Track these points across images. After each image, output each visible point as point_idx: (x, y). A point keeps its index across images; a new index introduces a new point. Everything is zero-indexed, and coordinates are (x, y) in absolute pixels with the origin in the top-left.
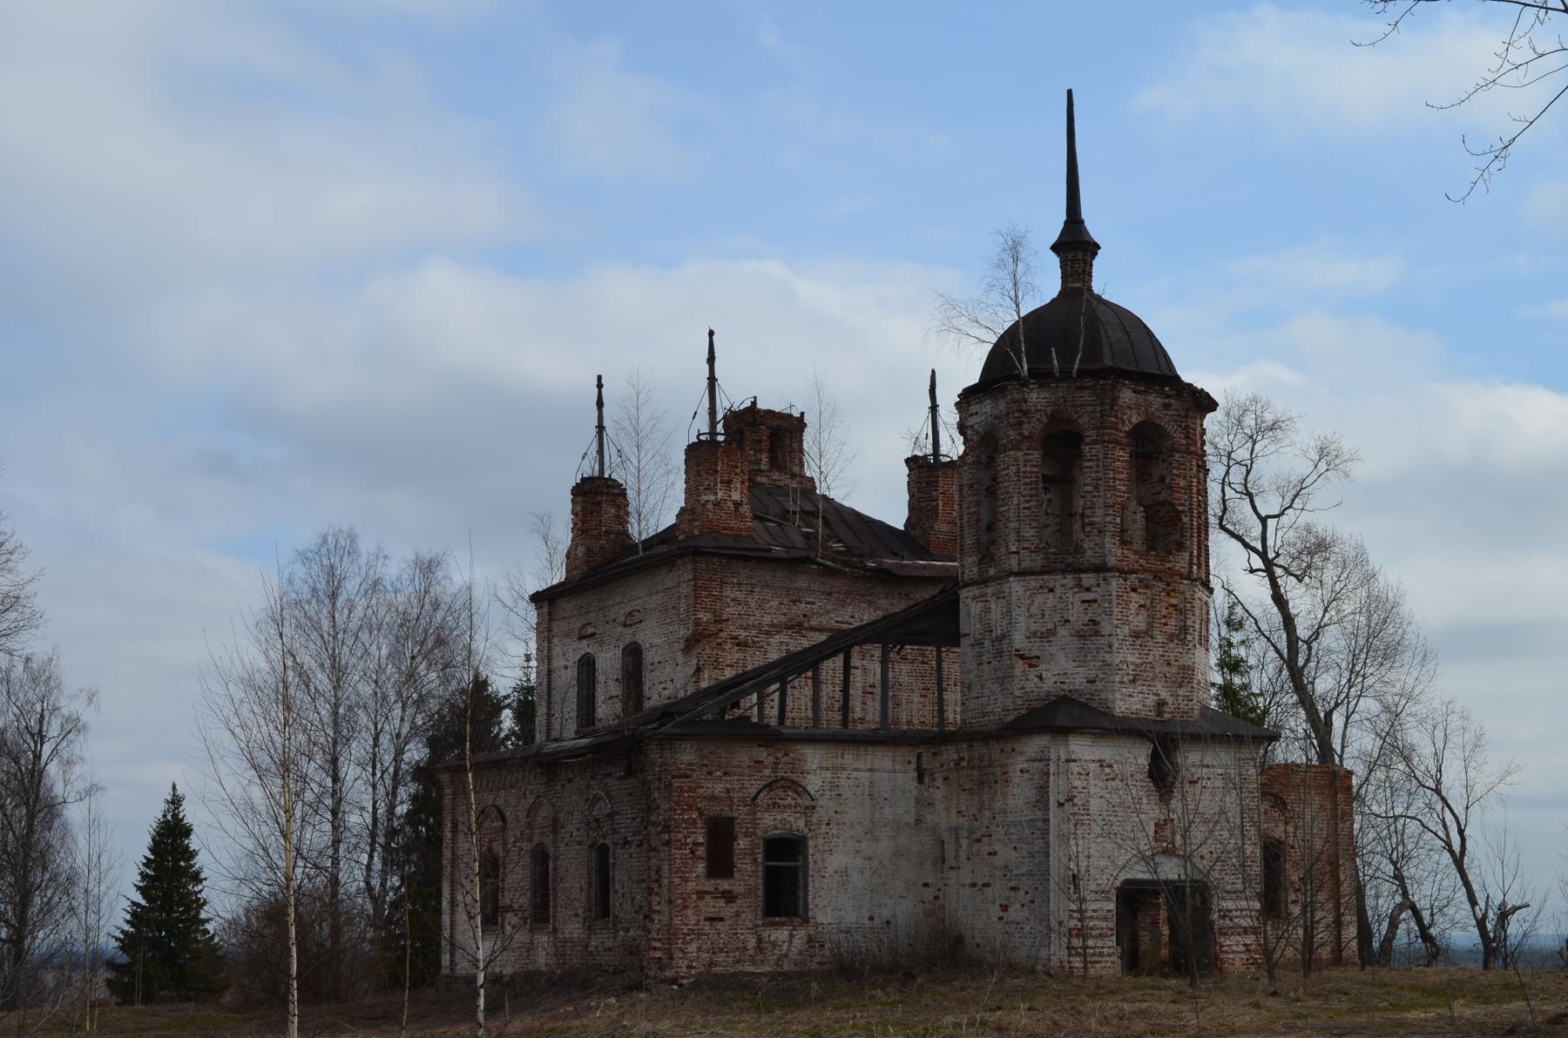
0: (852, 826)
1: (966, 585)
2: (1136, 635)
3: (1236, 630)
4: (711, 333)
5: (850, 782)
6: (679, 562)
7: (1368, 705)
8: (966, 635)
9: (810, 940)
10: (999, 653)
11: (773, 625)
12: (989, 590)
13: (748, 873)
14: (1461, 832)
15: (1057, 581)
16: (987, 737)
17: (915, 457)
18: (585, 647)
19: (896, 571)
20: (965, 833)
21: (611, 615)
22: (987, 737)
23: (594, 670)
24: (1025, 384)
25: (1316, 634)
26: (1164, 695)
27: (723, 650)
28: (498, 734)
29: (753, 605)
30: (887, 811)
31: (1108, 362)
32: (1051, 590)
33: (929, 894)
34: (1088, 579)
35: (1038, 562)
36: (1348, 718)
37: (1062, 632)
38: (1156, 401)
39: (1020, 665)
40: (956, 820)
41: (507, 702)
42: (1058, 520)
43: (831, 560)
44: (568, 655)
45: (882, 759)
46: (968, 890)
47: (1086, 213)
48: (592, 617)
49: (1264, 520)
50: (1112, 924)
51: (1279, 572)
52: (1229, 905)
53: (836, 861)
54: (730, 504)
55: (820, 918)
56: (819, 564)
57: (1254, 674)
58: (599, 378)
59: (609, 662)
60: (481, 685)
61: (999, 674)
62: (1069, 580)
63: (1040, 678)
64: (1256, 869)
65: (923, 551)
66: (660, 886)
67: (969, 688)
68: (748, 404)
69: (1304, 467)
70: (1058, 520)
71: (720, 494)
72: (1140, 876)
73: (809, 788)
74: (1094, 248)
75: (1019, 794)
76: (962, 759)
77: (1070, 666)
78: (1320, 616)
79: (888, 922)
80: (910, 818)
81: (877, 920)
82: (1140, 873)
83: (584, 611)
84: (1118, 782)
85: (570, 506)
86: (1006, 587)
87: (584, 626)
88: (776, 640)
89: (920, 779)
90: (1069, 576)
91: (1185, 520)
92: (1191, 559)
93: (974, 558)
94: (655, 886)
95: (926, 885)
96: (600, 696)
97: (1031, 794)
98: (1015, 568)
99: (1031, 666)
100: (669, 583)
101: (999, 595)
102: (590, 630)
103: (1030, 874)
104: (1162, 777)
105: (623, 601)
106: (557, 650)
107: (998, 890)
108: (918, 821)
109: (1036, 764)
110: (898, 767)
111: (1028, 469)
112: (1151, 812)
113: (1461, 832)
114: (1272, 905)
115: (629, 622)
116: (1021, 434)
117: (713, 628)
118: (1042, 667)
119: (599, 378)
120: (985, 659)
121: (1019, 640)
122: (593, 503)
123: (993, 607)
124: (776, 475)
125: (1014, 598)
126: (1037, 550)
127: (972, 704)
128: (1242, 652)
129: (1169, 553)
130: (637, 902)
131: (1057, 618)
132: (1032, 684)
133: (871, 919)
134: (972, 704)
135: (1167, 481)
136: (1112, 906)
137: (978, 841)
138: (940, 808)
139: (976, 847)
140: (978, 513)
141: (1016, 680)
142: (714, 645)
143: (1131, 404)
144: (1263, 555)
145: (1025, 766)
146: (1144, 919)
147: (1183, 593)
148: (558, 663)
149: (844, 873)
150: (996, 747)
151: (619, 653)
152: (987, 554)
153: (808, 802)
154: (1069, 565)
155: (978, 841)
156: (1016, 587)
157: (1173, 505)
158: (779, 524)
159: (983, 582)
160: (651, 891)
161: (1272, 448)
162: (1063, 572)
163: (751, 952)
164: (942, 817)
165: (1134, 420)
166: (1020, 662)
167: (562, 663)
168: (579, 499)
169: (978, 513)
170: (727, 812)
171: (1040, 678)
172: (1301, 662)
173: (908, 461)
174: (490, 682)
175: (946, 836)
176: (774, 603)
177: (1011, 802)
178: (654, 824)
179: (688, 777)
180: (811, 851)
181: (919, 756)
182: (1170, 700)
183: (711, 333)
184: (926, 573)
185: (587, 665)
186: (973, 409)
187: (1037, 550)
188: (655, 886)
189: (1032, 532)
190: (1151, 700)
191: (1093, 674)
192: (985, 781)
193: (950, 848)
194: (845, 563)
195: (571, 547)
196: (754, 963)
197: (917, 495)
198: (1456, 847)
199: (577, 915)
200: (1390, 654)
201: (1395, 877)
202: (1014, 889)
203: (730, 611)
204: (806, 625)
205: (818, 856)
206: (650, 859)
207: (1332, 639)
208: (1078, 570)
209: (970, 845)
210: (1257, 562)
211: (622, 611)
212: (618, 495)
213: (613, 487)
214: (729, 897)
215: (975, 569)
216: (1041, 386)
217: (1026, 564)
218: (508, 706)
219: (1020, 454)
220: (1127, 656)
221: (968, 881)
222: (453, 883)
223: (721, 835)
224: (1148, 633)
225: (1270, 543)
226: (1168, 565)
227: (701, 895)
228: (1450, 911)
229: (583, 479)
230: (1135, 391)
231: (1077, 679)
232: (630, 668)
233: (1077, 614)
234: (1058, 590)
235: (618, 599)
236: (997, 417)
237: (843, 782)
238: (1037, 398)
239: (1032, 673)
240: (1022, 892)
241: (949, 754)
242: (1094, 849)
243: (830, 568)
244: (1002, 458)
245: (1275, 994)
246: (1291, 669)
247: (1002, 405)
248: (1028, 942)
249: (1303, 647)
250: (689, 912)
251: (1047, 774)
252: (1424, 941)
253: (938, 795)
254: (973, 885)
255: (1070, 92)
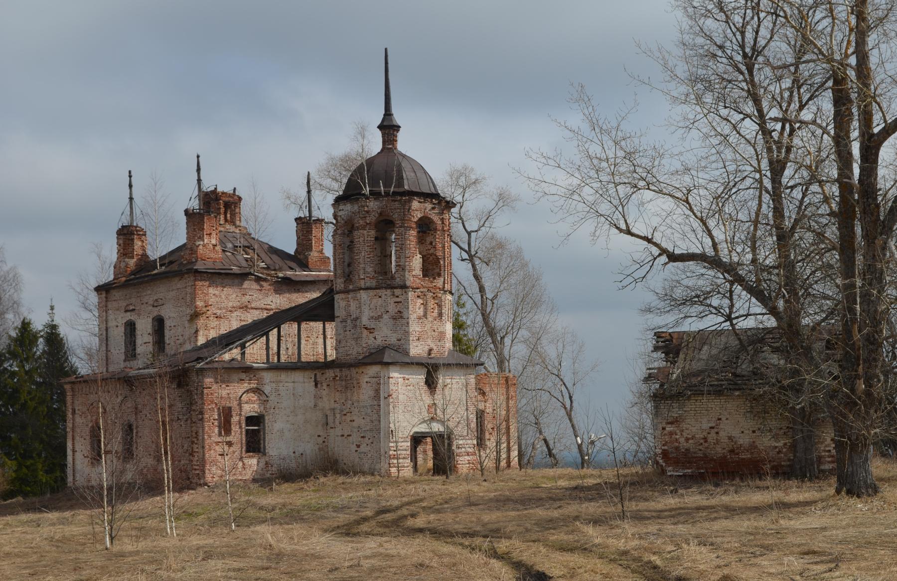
0: (285, 409)
1: (338, 293)
2: (419, 318)
3: (462, 307)
4: (198, 157)
5: (284, 388)
6: (186, 276)
7: (524, 333)
8: (337, 317)
9: (267, 462)
10: (355, 326)
11: (234, 307)
12: (350, 296)
13: (238, 434)
14: (571, 398)
15: (382, 292)
16: (350, 366)
17: (300, 217)
18: (129, 316)
19: (293, 278)
20: (339, 411)
21: (145, 300)
22: (350, 366)
23: (135, 329)
24: (367, 198)
25: (496, 297)
26: (433, 345)
27: (209, 320)
28: (36, 352)
29: (223, 297)
30: (301, 402)
31: (406, 187)
32: (380, 297)
33: (320, 440)
34: (398, 292)
35: (374, 283)
36: (512, 341)
37: (385, 316)
38: (429, 206)
39: (365, 332)
40: (333, 405)
41: (42, 334)
42: (379, 258)
43: (261, 273)
44: (118, 321)
45: (298, 376)
46: (340, 438)
47: (394, 110)
48: (133, 300)
49: (469, 233)
50: (409, 452)
51: (477, 261)
52: (461, 442)
53: (278, 426)
54: (211, 246)
55: (271, 453)
56: (255, 276)
57: (470, 330)
58: (130, 172)
59: (144, 327)
60: (25, 326)
61: (355, 336)
62: (389, 292)
63: (375, 338)
64: (473, 425)
65: (304, 265)
66: (198, 440)
67: (340, 342)
68: (212, 188)
69: (490, 204)
70: (379, 258)
71: (206, 241)
72: (423, 430)
73: (265, 392)
74: (398, 128)
75: (365, 393)
76: (337, 376)
77: (389, 333)
78: (498, 285)
79: (302, 454)
80: (312, 404)
81: (297, 454)
82: (423, 428)
83: (127, 297)
84: (411, 387)
85: (116, 240)
86: (358, 295)
87: (128, 305)
88: (235, 314)
89: (316, 385)
90: (389, 291)
91: (442, 262)
92: (444, 281)
93: (342, 280)
94: (195, 440)
95: (319, 436)
96: (139, 341)
97: (372, 393)
98: (363, 286)
99: (370, 333)
100: (179, 286)
101: (354, 299)
102: (131, 308)
103: (371, 430)
104: (431, 384)
105: (151, 294)
106: (111, 317)
107: (355, 438)
108: (315, 406)
109: (374, 379)
110: (306, 380)
111: (369, 239)
112: (428, 400)
113: (571, 398)
114: (481, 443)
115: (155, 304)
116: (366, 222)
117: (204, 309)
118: (376, 333)
119: (130, 172)
120: (348, 329)
121: (365, 320)
122: (129, 240)
123: (352, 304)
124: (228, 226)
125: (362, 300)
126: (373, 278)
127: (341, 350)
128: (464, 318)
129: (434, 278)
130: (185, 448)
131: (383, 310)
132: (371, 341)
133: (294, 453)
134: (341, 350)
135: (434, 244)
136: (409, 444)
137: (345, 415)
138: (325, 399)
139: (344, 417)
140: (344, 258)
141: (363, 340)
142: (205, 318)
143: (418, 209)
144: (468, 252)
145: (368, 380)
146: (420, 449)
147: (441, 298)
148: (111, 324)
149: (282, 431)
150: (354, 371)
151: (150, 320)
152: (348, 277)
153: (265, 398)
154: (388, 285)
155: (345, 415)
156: (363, 295)
157: (435, 255)
158: (233, 254)
159: (346, 291)
160: (193, 442)
161: (474, 195)
162: (386, 288)
163: (240, 470)
164: (326, 403)
165: (419, 216)
166: (366, 331)
167: (115, 323)
168: (122, 237)
169: (344, 258)
170: (228, 405)
171: (375, 338)
172: (488, 310)
173: (296, 219)
174: (32, 322)
175: (328, 413)
176: (234, 296)
177: (361, 397)
178: (194, 410)
179: (210, 388)
180: (266, 421)
181: (315, 375)
182: (435, 348)
183: (198, 157)
184: (308, 279)
185: (131, 328)
186: (341, 207)
187: (373, 278)
188: (195, 440)
189: (371, 269)
190: (426, 349)
191: (400, 337)
192: (349, 386)
193: (330, 419)
194: (268, 275)
195: (116, 262)
196: (241, 474)
197: (301, 237)
198: (568, 406)
199: (150, 455)
200: (536, 304)
201: (536, 424)
202: (363, 437)
203: (212, 300)
204: (249, 306)
205: (269, 424)
206: (192, 427)
207: (503, 299)
208: (392, 287)
209: (341, 417)
210: (465, 256)
211: (152, 299)
212: (143, 235)
213: (139, 231)
214: (230, 444)
215: (342, 286)
216: (375, 199)
217: (368, 284)
218: (42, 336)
219: (365, 232)
220: (415, 328)
221: (340, 434)
222: (73, 439)
223: (226, 416)
224: (425, 315)
225: (473, 244)
226: (434, 284)
227: (217, 443)
228: (564, 441)
229: (123, 227)
230: (419, 202)
231: (393, 339)
232: (156, 328)
233: (392, 309)
234: (383, 297)
235: (149, 292)
236: (353, 213)
237: (281, 388)
238: (373, 205)
239: (371, 336)
240: (367, 439)
241: (330, 373)
242: (401, 417)
243: (261, 278)
244: (356, 233)
245: (485, 480)
246: (483, 315)
247: (356, 207)
248: (370, 462)
249: (489, 302)
250: (212, 451)
251: (379, 384)
252: (550, 456)
253: (324, 393)
254: (343, 436)
255: (386, 50)
